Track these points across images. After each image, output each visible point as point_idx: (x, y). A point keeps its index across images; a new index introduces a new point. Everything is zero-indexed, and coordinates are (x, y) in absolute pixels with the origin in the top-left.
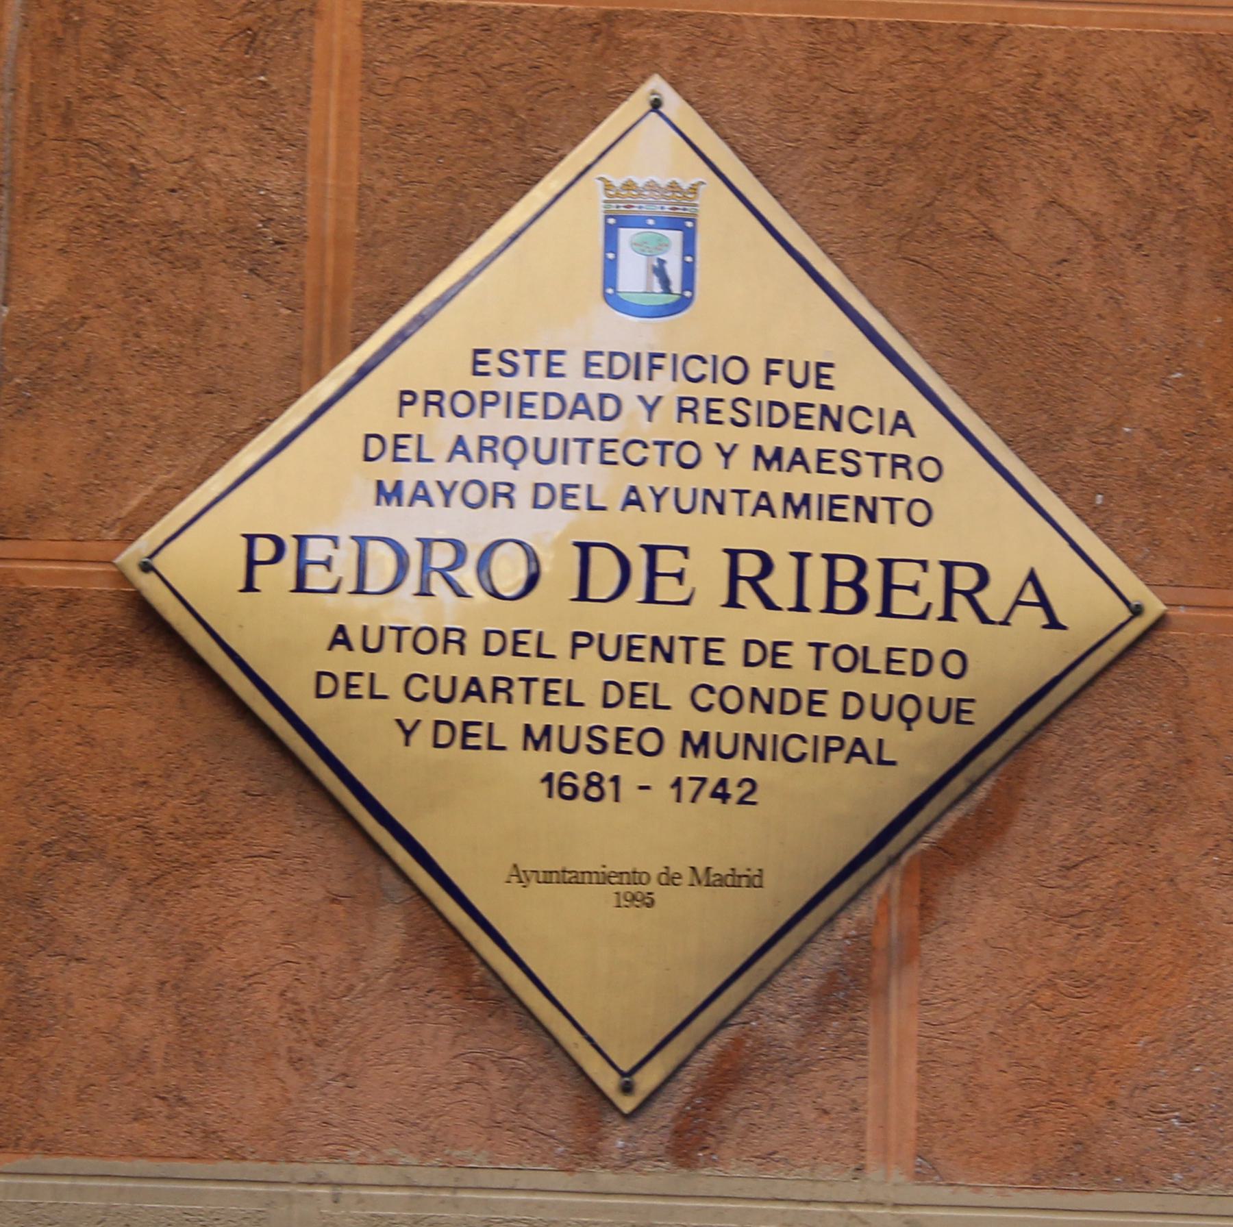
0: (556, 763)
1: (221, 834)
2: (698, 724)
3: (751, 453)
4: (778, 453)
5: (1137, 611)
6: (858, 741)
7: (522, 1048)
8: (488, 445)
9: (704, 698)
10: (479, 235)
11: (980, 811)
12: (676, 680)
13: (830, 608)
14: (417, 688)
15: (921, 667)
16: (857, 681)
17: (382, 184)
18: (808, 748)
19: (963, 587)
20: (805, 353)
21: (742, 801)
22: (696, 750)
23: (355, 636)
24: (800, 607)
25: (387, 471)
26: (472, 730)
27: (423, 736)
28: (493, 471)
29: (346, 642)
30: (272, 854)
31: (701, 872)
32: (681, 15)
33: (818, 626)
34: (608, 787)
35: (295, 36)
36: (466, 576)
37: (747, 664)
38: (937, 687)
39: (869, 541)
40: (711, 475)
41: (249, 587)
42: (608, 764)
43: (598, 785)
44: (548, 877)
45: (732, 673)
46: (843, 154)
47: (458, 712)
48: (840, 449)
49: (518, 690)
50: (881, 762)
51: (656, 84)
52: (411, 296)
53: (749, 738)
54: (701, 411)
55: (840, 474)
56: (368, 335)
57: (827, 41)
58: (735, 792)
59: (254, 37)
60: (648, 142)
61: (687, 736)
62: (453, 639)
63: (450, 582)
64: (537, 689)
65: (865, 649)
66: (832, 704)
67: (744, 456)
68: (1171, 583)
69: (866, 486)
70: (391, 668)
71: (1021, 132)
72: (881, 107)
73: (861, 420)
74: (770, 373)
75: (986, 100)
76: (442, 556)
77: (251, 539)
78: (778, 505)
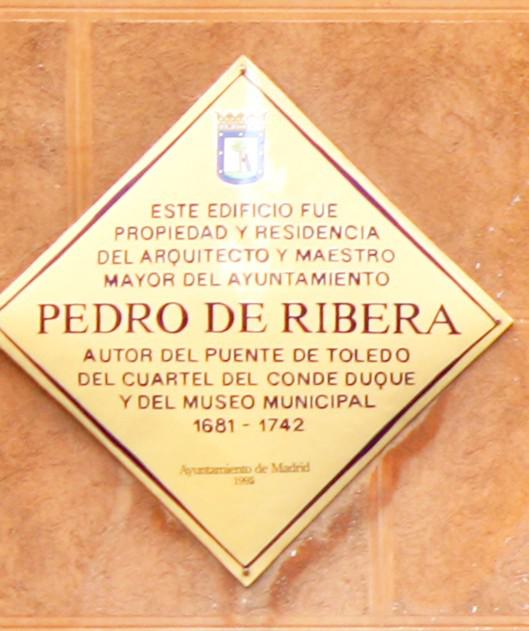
0: (200, 414)
1: (37, 454)
2: (272, 393)
3: (295, 252)
4: (308, 253)
5: (497, 323)
6: (355, 397)
7: (193, 555)
8: (160, 254)
9: (274, 379)
10: (155, 141)
11: (422, 427)
12: (259, 370)
13: (337, 330)
14: (129, 379)
15: (386, 358)
16: (353, 366)
17: (106, 118)
18: (329, 401)
19: (406, 317)
20: (321, 202)
21: (296, 429)
22: (271, 405)
23: (96, 354)
24: (322, 330)
25: (111, 270)
26: (157, 399)
27: (133, 403)
28: (163, 267)
29: (91, 357)
30: (64, 463)
31: (277, 466)
32: (253, 23)
33: (331, 339)
34: (228, 425)
35: (56, 43)
36: (152, 321)
37: (295, 360)
38: (395, 368)
39: (358, 296)
40: (274, 266)
41: (42, 330)
42: (227, 414)
43: (222, 424)
44: (200, 471)
45: (288, 365)
46: (342, 92)
47: (151, 390)
48: (340, 249)
49: (180, 378)
50: (368, 406)
51: (244, 61)
52: (121, 175)
53: (298, 398)
54: (268, 232)
55: (341, 262)
56: (100, 196)
57: (333, 34)
58: (293, 425)
59: (36, 44)
60: (244, 93)
61: (267, 399)
62: (147, 354)
63: (143, 325)
64: (189, 378)
65: (356, 351)
66: (340, 379)
67: (291, 255)
68: (516, 308)
69: (355, 267)
70: (115, 370)
71: (432, 77)
72: (360, 67)
73: (351, 232)
74: (304, 211)
75: (414, 61)
76: (139, 312)
77: (43, 307)
78: (309, 278)
